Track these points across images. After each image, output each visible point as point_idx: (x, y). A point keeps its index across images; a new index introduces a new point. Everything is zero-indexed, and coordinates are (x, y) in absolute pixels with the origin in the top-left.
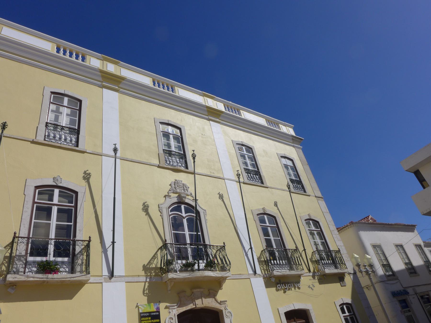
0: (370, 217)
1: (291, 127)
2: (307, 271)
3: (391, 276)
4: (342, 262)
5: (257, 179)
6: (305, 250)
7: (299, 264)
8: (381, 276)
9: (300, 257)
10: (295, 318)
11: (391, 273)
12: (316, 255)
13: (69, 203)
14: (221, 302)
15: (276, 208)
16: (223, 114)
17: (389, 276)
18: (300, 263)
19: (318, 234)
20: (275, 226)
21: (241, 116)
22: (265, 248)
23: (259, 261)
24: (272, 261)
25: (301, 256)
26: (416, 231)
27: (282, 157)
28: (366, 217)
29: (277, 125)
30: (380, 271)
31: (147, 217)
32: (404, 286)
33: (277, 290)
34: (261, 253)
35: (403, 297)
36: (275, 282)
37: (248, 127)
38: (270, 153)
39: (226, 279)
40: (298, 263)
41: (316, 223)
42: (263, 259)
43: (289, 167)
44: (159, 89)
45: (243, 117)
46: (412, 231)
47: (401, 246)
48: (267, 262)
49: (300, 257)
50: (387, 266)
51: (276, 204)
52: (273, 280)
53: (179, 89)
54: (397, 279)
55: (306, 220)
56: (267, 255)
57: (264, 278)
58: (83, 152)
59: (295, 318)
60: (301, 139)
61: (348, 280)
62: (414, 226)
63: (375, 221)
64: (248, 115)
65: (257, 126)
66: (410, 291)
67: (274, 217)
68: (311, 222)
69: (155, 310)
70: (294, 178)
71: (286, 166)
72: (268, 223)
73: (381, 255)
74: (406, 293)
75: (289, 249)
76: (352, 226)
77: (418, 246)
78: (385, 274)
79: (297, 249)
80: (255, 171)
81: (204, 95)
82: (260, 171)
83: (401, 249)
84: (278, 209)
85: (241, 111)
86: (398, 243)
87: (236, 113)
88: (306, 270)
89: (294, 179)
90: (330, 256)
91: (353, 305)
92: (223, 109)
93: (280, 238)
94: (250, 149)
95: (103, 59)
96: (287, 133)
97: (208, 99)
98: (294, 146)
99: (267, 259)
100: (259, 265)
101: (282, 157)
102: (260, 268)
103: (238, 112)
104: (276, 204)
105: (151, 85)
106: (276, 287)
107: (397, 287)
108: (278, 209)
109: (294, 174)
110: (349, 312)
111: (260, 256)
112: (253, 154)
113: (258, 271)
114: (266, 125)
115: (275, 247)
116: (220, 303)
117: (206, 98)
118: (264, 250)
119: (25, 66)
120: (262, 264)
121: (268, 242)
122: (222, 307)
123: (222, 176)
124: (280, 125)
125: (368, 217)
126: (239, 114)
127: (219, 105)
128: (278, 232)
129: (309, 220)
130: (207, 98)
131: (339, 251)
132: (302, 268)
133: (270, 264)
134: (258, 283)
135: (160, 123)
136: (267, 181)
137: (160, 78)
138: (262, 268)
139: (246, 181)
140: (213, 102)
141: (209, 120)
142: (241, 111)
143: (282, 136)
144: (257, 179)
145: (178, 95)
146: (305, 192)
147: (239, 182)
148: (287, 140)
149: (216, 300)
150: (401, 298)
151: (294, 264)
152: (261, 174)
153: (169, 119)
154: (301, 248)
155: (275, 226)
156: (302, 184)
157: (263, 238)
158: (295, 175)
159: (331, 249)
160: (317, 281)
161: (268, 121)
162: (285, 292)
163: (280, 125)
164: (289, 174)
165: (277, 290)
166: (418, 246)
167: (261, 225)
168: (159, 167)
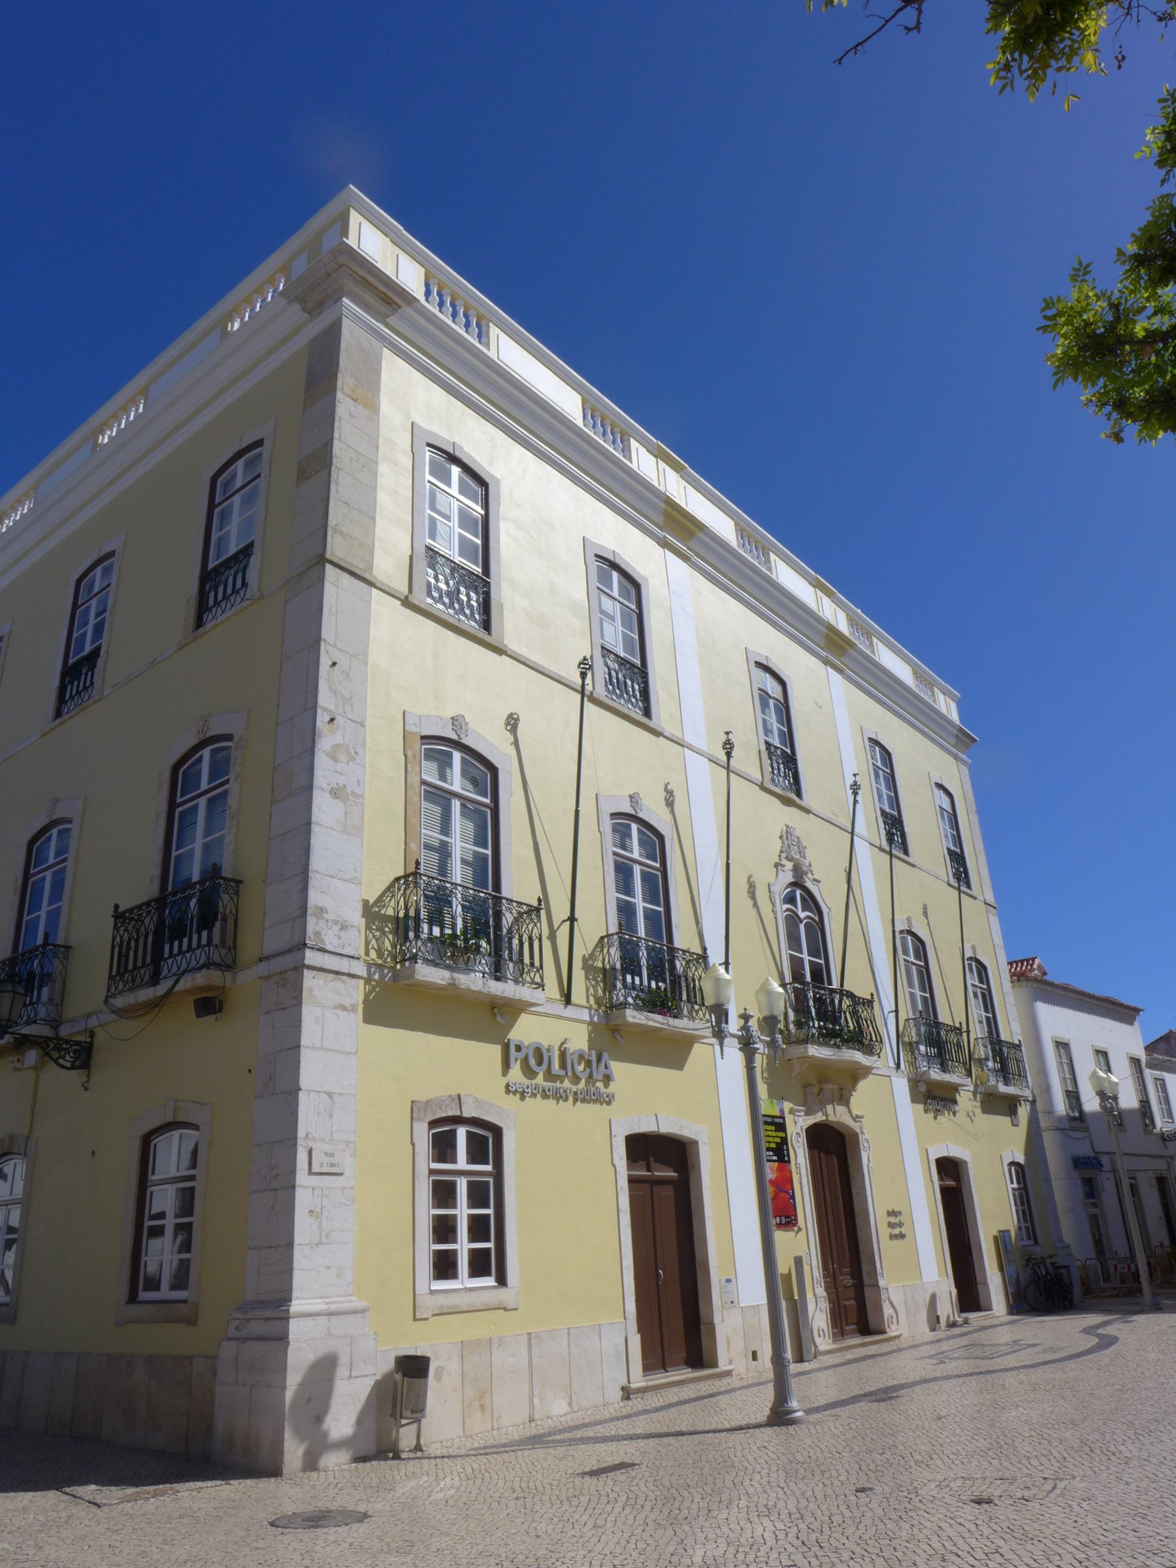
0: (1037, 961)
1: (952, 697)
2: (557, 995)
3: (1078, 1120)
4: (1022, 1075)
5: (635, 697)
6: (572, 919)
7: (532, 964)
8: (1060, 1118)
9: (547, 944)
10: (652, 1159)
11: (1077, 1114)
12: (613, 950)
13: (648, 857)
14: (857, 1117)
15: (667, 810)
16: (701, 535)
17: (1074, 1119)
18: (537, 963)
19: (645, 877)
20: (658, 865)
21: (488, 346)
22: (613, 929)
23: (588, 968)
24: (425, 927)
25: (553, 937)
26: (1136, 1023)
27: (759, 665)
28: (1028, 960)
29: (868, 634)
30: (1061, 1106)
31: (754, 912)
32: (1097, 1149)
33: (926, 1111)
34: (392, 885)
35: (1088, 1173)
36: (935, 1098)
37: (806, 631)
38: (837, 717)
39: (523, 1010)
40: (527, 960)
41: (982, 969)
42: (600, 965)
43: (771, 702)
44: (466, 335)
45: (492, 354)
46: (1130, 1022)
47: (1105, 1054)
48: (608, 977)
49: (547, 944)
50: (1073, 1096)
51: (512, 723)
52: (922, 1088)
53: (503, 336)
54: (1086, 1130)
55: (614, 815)
56: (615, 954)
57: (909, 1081)
58: (657, 733)
59: (652, 1159)
60: (974, 740)
61: (1023, 1111)
62: (1137, 1011)
63: (1045, 974)
64: (789, 577)
65: (785, 600)
66: (1105, 1160)
67: (494, 770)
68: (634, 827)
69: (778, 1114)
70: (776, 742)
71: (764, 696)
72: (805, 917)
73: (1066, 1067)
74: (1099, 1165)
75: (510, 901)
76: (1023, 984)
77: (1135, 1061)
78: (1068, 1115)
79: (703, 957)
80: (892, 816)
81: (817, 585)
82: (493, 580)
83: (1101, 1059)
84: (516, 743)
85: (494, 331)
86: (1102, 1046)
87: (614, 442)
88: (553, 989)
89: (888, 810)
90: (1005, 1058)
91: (1026, 1170)
92: (418, 292)
93: (489, 852)
94: (633, 585)
95: (656, 452)
96: (655, 483)
97: (669, 470)
98: (956, 757)
99: (406, 915)
100: (587, 978)
101: (759, 665)
102: (588, 990)
103: (479, 326)
104: (512, 723)
105: (418, 292)
106: (925, 1103)
107: (1084, 1150)
108: (516, 743)
109: (779, 729)
110: (1019, 1183)
111: (594, 950)
112: (486, 506)
113: (578, 995)
114: (579, 422)
115: (642, 932)
116: (856, 1118)
117: (662, 465)
118: (608, 936)
119: (417, 376)
120: (595, 979)
121: (626, 911)
122: (856, 1127)
123: (680, 736)
124: (773, 557)
125: (1033, 959)
126: (482, 335)
127: (717, 519)
128: (657, 887)
129: (440, 746)
130: (664, 465)
131: (1019, 1046)
132: (538, 979)
133: (619, 985)
134: (901, 1086)
135: (597, 556)
136: (512, 625)
137: (462, 287)
138: (591, 990)
139: (601, 692)
140: (678, 483)
141: (664, 544)
142: (494, 331)
143: (940, 725)
144: (635, 697)
145: (494, 357)
146: (647, 712)
147: (728, 768)
148: (776, 609)
149: (850, 1112)
150: (1088, 1173)
151: (511, 959)
152: (493, 595)
153: (457, 440)
154: (560, 911)
155: (487, 801)
156: (796, 768)
157: (613, 895)
158: (781, 734)
159: (678, 943)
160: (978, 1104)
161: (741, 531)
162: (935, 1118)
163: (773, 557)
164: (767, 731)
165: (926, 1111)
166: (1135, 1061)
167: (615, 854)
168: (406, 603)
